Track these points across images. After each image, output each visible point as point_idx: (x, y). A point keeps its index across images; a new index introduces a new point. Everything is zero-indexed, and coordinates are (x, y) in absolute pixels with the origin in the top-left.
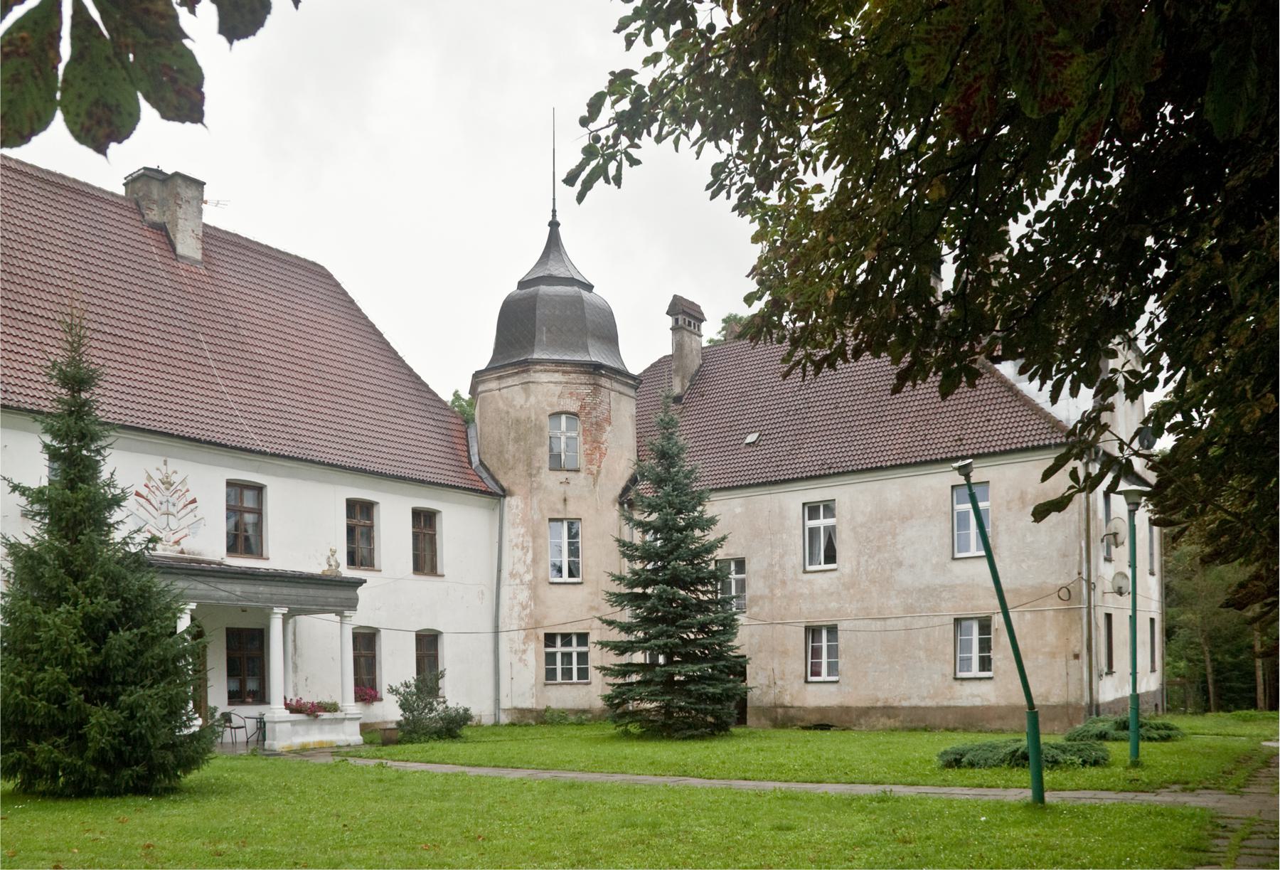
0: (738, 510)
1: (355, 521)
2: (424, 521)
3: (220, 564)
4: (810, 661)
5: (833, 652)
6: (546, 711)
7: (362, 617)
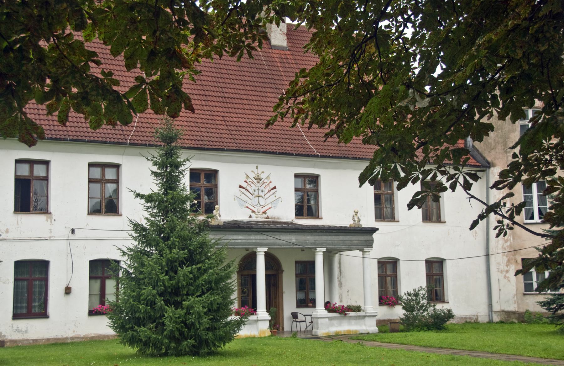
1: (380, 192)
3: (292, 223)
6: (525, 313)
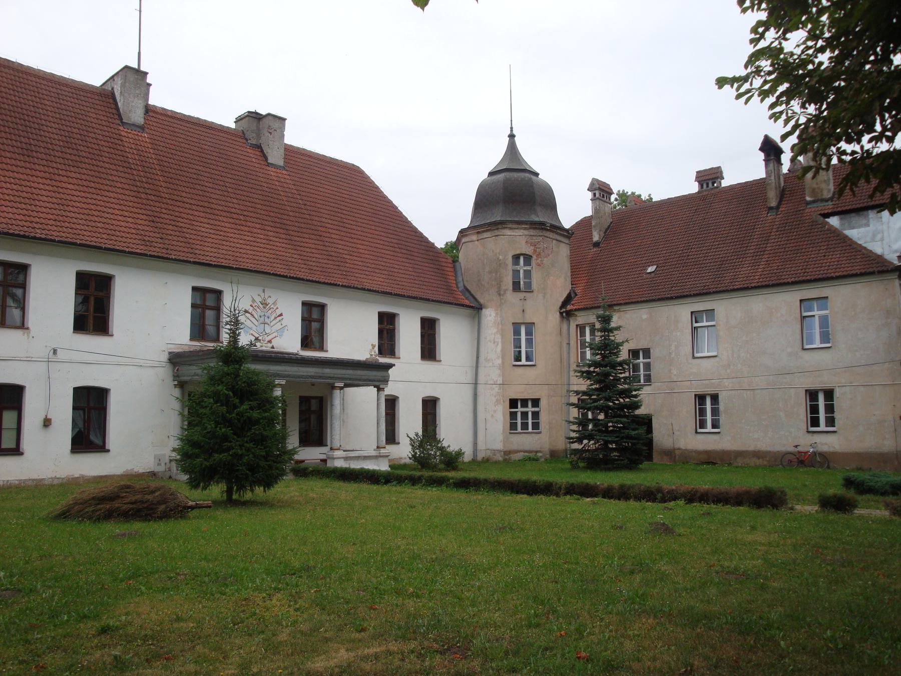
0: (645, 317)
2: (429, 328)
4: (809, 415)
5: (715, 412)
7: (389, 390)
